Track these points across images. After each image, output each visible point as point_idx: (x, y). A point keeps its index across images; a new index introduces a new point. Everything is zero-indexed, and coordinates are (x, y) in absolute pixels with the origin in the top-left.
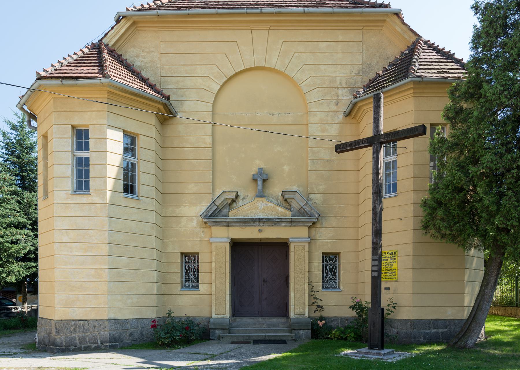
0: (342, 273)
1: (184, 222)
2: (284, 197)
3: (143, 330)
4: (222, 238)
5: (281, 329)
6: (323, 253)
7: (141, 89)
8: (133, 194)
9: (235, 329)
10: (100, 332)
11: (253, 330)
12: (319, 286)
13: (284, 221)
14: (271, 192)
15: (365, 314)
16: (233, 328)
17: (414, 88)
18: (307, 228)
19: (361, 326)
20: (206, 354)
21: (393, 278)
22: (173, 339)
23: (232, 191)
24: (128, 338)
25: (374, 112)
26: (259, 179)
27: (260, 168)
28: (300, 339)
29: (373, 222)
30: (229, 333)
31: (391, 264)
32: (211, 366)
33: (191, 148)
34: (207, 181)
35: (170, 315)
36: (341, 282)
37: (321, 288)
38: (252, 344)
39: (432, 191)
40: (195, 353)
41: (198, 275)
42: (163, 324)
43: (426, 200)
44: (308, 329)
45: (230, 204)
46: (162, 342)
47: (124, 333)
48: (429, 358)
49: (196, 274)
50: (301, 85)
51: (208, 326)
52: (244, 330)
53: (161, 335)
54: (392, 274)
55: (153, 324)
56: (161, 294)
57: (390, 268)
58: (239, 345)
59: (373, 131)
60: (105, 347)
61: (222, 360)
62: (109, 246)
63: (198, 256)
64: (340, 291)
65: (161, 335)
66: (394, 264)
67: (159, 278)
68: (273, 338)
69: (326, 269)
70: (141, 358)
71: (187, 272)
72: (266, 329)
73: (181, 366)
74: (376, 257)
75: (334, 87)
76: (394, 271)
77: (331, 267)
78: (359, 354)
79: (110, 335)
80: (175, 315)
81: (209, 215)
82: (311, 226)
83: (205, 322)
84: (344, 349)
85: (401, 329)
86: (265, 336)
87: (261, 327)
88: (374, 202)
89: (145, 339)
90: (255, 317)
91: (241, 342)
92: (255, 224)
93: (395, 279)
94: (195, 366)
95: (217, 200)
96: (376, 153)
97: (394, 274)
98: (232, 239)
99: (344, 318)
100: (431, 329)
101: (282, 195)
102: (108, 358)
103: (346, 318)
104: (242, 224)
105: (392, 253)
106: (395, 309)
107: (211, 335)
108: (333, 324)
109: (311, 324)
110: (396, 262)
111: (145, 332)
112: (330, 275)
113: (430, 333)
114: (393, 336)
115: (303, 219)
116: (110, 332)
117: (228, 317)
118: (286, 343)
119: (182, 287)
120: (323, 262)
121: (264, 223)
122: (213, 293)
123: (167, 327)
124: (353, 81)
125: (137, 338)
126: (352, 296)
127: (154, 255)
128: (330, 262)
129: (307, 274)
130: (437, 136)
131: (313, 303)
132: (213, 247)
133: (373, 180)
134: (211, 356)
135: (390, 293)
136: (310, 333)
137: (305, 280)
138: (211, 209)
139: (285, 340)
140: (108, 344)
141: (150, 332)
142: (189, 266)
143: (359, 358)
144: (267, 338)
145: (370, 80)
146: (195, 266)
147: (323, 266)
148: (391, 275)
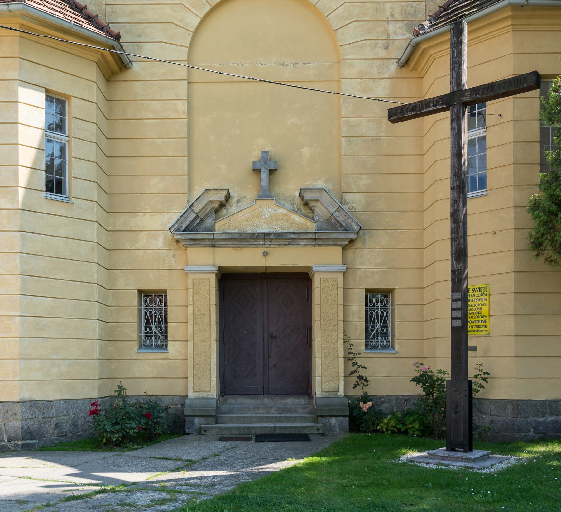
0: (397, 323)
1: (143, 240)
2: (303, 199)
3: (77, 419)
4: (205, 266)
5: (300, 415)
6: (367, 291)
7: (74, 22)
8: (61, 194)
9: (225, 417)
10: (6, 421)
11: (255, 417)
12: (360, 345)
13: (303, 237)
14: (282, 190)
15: (438, 391)
16: (222, 414)
17: (512, 17)
18: (340, 248)
19: (431, 410)
20: (180, 460)
21: (482, 331)
22: (125, 434)
23: (220, 188)
24: (52, 431)
25: (453, 52)
26: (263, 170)
27: (265, 152)
28: (331, 433)
29: (453, 236)
30: (217, 423)
31: (479, 307)
32: (188, 482)
33: (155, 120)
34: (180, 173)
35: (120, 393)
36: (396, 337)
37: (363, 347)
38: (253, 441)
39: (547, 184)
40: (162, 458)
41: (166, 327)
42: (110, 408)
43: (536, 200)
44: (345, 416)
45: (217, 211)
46: (108, 438)
47: (45, 423)
48: (550, 466)
49: (163, 326)
50: (328, 17)
51: (183, 411)
52: (240, 417)
53: (106, 427)
54: (480, 324)
55: (93, 408)
56: (106, 359)
57: (476, 315)
58: (232, 442)
59: (452, 84)
60: (15, 447)
61: (205, 470)
62: (22, 278)
63: (166, 296)
64: (395, 352)
65: (106, 427)
66: (483, 307)
67: (103, 333)
68: (288, 432)
69: (371, 317)
70: (72, 467)
71: (148, 322)
72: (277, 415)
73: (138, 481)
74: (458, 295)
75: (381, 19)
76: (483, 319)
77: (380, 313)
78: (433, 459)
79: (22, 427)
80: (128, 393)
81: (184, 228)
82: (346, 245)
83: (177, 405)
84: (405, 450)
85: (497, 416)
86: (275, 428)
87: (267, 412)
88: (454, 202)
89: (80, 433)
90: (257, 396)
91: (236, 438)
92: (257, 243)
93: (485, 333)
94: (162, 481)
95: (195, 204)
96: (456, 121)
97: (483, 324)
98: (220, 268)
99: (401, 397)
100: (547, 415)
101: (300, 195)
102: (18, 467)
103: (405, 397)
104: (235, 243)
105: (480, 289)
106: (487, 382)
107: (187, 426)
108: (384, 407)
109: (349, 407)
110: (487, 304)
111: (80, 420)
112: (379, 326)
113: (544, 422)
114: (484, 428)
115: (335, 235)
116: (23, 422)
117: (215, 396)
118: (309, 440)
119: (140, 347)
120: (366, 305)
121: (271, 242)
122: (190, 356)
123: (116, 413)
124: (412, 10)
125: (66, 433)
126: (415, 361)
127: (95, 293)
128: (377, 304)
129: (342, 324)
130: (555, 93)
131: (352, 373)
132: (190, 281)
133: (452, 165)
134: (187, 463)
135: (478, 356)
136: (348, 423)
137: (338, 335)
138: (187, 218)
139: (307, 435)
140: (19, 442)
141: (88, 422)
142: (151, 312)
143: (434, 467)
144: (278, 432)
145: (440, 7)
146: (161, 313)
147: (366, 312)
148: (479, 327)
